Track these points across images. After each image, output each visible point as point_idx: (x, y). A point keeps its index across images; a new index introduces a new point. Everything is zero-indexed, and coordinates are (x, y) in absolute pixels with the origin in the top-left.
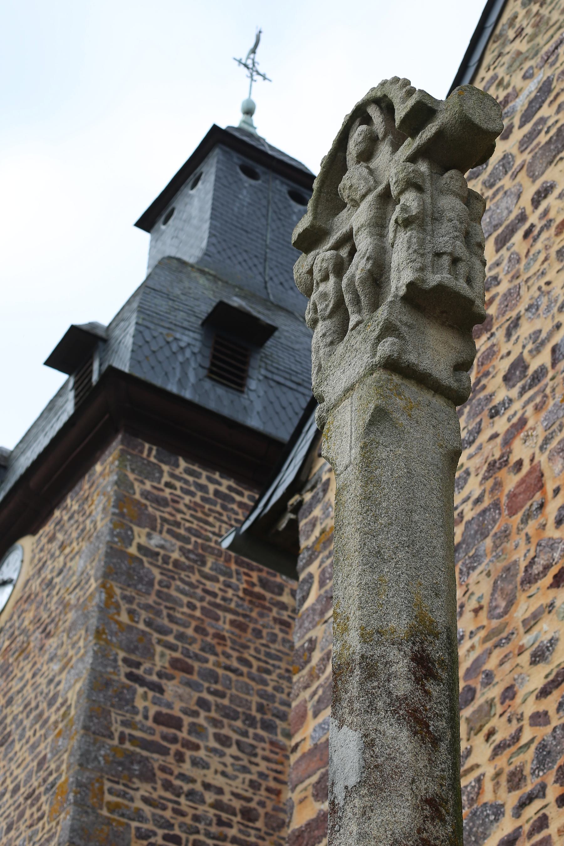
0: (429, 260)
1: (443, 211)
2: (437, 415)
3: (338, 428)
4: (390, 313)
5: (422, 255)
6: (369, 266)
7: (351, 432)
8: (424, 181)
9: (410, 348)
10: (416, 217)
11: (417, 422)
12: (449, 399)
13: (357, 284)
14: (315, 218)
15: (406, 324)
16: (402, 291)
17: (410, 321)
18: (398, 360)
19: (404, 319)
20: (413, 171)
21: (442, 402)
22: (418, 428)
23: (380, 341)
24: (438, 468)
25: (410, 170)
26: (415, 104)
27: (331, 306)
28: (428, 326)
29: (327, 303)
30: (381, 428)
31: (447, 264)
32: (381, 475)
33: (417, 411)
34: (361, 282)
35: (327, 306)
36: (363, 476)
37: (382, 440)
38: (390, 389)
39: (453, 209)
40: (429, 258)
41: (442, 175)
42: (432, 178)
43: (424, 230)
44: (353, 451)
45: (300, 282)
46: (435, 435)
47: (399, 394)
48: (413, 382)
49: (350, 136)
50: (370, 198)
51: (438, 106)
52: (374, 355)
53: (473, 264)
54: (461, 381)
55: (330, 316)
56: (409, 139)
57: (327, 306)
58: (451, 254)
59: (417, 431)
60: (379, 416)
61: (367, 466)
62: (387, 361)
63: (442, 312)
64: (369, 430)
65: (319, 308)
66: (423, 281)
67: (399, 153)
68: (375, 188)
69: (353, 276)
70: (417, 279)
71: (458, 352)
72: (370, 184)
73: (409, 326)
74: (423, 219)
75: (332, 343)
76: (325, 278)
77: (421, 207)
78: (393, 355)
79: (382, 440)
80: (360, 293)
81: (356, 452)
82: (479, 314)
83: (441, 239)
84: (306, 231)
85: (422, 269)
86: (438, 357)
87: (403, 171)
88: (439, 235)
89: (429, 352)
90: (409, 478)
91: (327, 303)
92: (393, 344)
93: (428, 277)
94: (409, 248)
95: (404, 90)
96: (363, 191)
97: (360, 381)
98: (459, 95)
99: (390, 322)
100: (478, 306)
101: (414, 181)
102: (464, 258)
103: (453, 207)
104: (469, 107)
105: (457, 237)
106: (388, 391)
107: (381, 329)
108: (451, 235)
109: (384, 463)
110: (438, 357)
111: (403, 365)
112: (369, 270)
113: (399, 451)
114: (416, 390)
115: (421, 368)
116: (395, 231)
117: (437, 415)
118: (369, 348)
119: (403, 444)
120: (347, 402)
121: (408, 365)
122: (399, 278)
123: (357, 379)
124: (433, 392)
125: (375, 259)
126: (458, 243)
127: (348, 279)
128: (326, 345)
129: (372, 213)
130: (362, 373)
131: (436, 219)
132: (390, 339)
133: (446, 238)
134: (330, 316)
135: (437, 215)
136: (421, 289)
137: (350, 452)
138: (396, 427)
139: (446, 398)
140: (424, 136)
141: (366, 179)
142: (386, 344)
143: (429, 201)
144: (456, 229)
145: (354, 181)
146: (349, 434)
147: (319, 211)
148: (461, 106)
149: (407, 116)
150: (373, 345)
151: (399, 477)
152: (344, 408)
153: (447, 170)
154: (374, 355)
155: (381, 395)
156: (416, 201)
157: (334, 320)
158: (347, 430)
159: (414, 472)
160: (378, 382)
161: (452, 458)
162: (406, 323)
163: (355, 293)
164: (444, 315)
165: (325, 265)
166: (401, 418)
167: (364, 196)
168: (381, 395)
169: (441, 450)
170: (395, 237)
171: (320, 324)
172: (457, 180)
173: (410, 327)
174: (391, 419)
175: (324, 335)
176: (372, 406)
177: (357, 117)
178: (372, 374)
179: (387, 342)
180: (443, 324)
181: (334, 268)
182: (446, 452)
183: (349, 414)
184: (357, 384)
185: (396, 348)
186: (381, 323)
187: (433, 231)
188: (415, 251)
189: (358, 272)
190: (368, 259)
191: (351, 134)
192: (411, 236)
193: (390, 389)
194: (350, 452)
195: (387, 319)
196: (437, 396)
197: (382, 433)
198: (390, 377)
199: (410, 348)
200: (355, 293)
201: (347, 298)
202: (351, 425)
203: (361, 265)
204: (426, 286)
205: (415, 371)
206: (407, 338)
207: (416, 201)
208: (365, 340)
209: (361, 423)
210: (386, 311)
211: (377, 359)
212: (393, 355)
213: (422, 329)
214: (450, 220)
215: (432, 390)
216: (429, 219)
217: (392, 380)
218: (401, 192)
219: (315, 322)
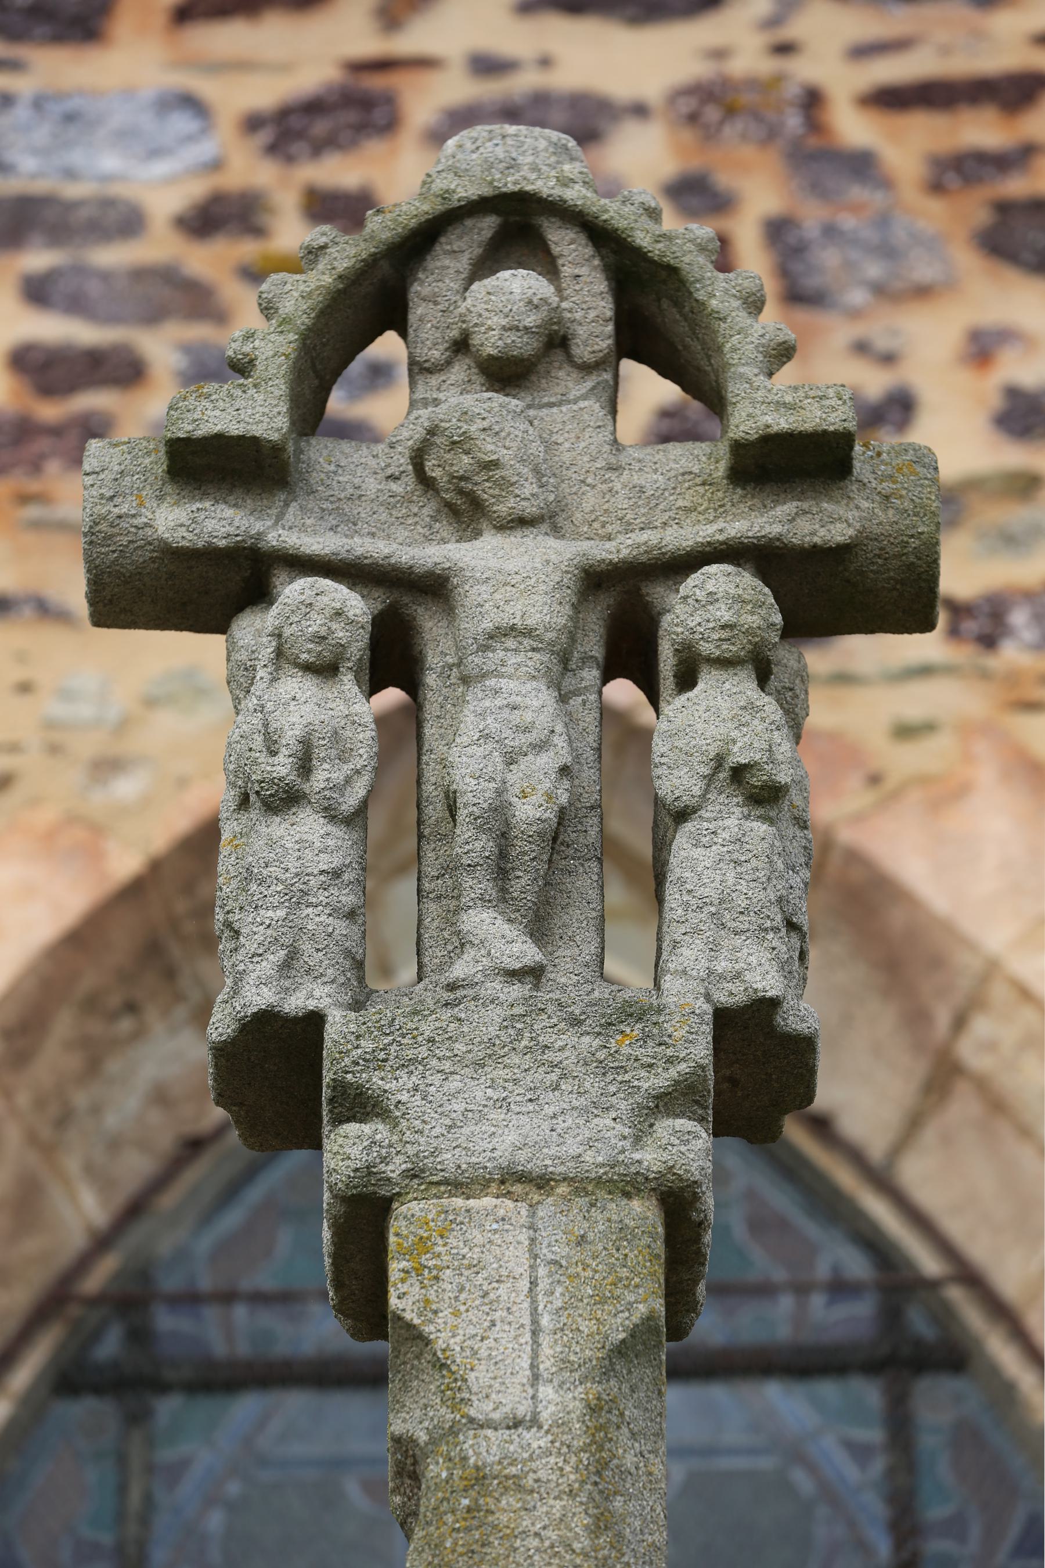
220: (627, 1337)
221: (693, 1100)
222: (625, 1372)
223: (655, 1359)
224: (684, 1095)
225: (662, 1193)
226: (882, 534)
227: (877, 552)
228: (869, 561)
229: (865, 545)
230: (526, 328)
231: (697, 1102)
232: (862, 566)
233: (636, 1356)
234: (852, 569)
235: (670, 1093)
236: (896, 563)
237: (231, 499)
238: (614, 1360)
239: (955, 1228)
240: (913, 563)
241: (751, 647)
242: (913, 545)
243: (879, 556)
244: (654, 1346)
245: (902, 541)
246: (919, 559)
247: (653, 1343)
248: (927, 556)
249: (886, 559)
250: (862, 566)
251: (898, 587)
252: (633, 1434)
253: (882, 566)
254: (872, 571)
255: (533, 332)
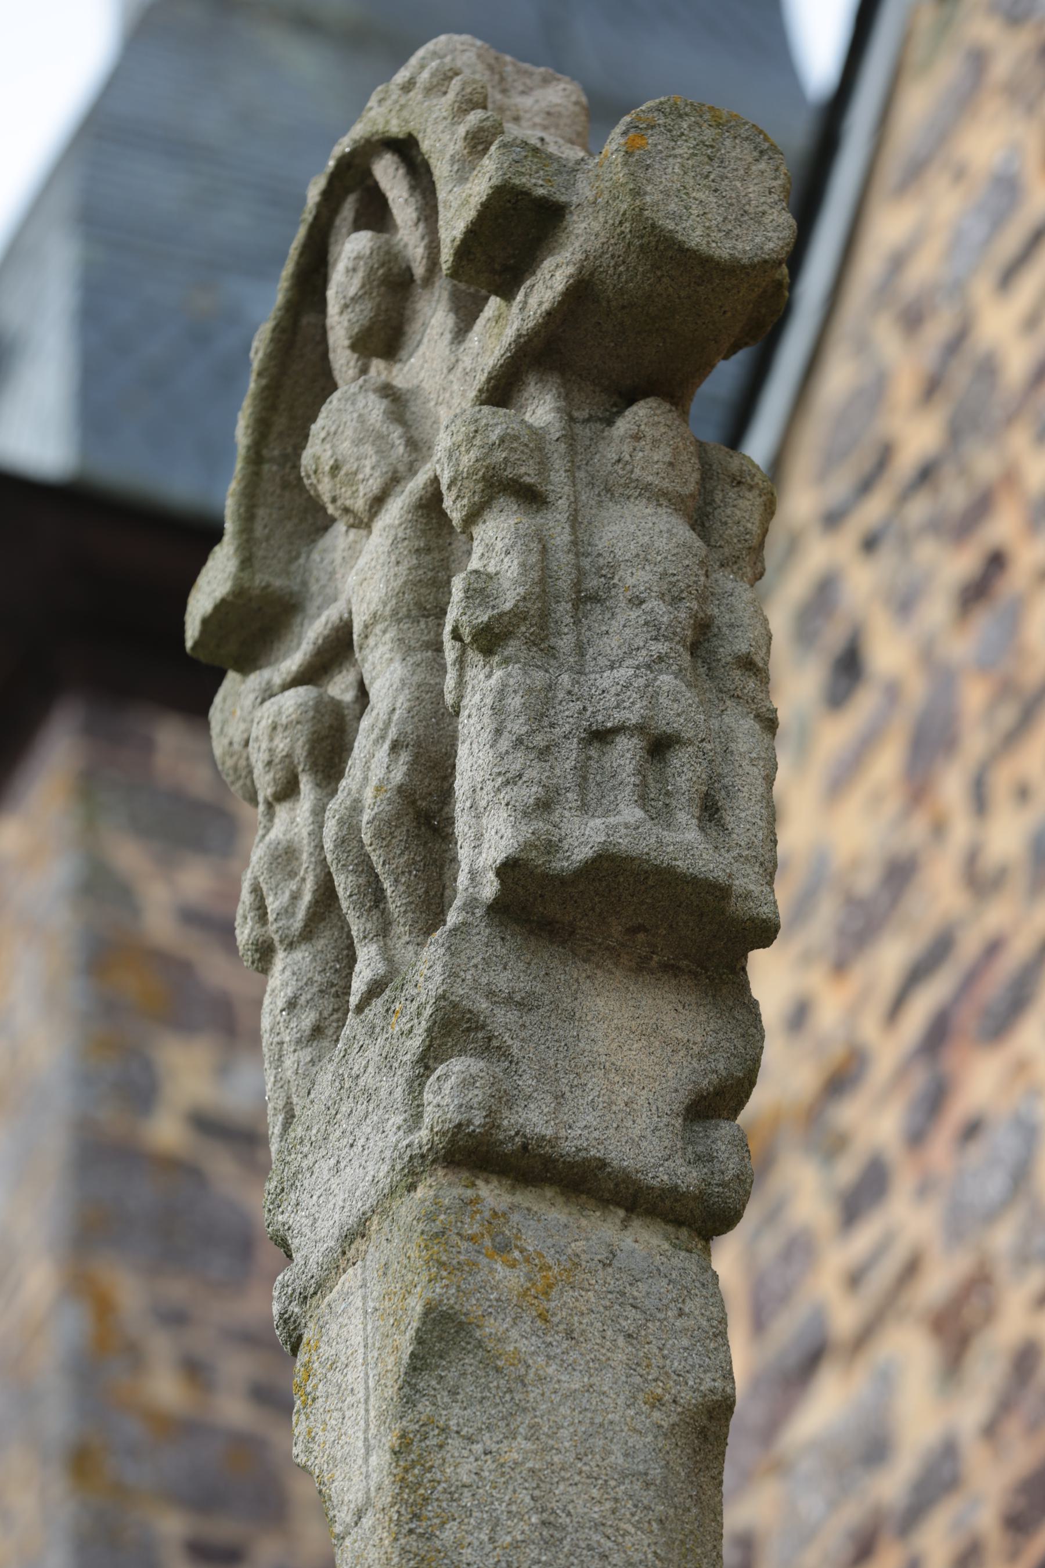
0: (569, 765)
1: (613, 567)
2: (638, 1292)
3: (333, 1367)
4: (452, 975)
5: (544, 753)
6: (398, 776)
7: (367, 1388)
8: (544, 466)
9: (527, 1082)
10: (518, 615)
11: (569, 1335)
12: (678, 1223)
13: (366, 839)
14: (246, 562)
15: (509, 1000)
16: (489, 889)
17: (523, 985)
18: (488, 1133)
19: (502, 981)
20: (502, 440)
21: (655, 1241)
22: (574, 1355)
23: (429, 1069)
24: (647, 1485)
25: (494, 437)
26: (490, 198)
27: (307, 897)
28: (586, 986)
29: (293, 885)
30: (452, 1376)
31: (630, 768)
32: (459, 1544)
33: (569, 1295)
34: (378, 835)
35: (295, 897)
36: (404, 1551)
37: (455, 1416)
38: (471, 1238)
39: (643, 557)
40: (570, 754)
41: (610, 422)
42: (572, 449)
43: (551, 652)
44: (374, 1460)
45: (235, 769)
46: (633, 1366)
47: (503, 1248)
48: (549, 1193)
49: (331, 259)
50: (395, 510)
51: (570, 185)
52: (416, 1119)
53: (727, 736)
54: (711, 1159)
55: (308, 934)
56: (494, 303)
57: (295, 897)
58: (641, 729)
59: (572, 1367)
60: (441, 1339)
61: (416, 1516)
62: (452, 1141)
63: (634, 930)
64: (413, 1386)
65: (273, 905)
66: (551, 847)
67: (474, 338)
68: (412, 470)
69: (356, 808)
70: (528, 846)
71: (700, 1056)
72: (393, 459)
73: (519, 1004)
74: (545, 614)
75: (317, 1032)
76: (288, 791)
77: (535, 575)
78: (469, 1122)
79: (455, 1416)
80: (379, 870)
81: (380, 1459)
82: (752, 920)
83: (607, 679)
84: (222, 607)
85: (544, 805)
86: (627, 1092)
87: (470, 440)
88: (603, 662)
89: (595, 1081)
90: (548, 1544)
91: (293, 885)
92: (468, 1082)
93: (566, 827)
94: (498, 732)
95: (462, 130)
96: (373, 485)
97: (381, 1207)
98: (628, 154)
99: (455, 1006)
100: (748, 896)
101: (509, 473)
102: (686, 735)
103: (646, 548)
104: (666, 193)
105: (660, 659)
106: (464, 1245)
107: (429, 1030)
108: (642, 657)
109: (467, 1500)
110: (627, 1092)
111: (509, 1148)
112: (400, 789)
113: (514, 1451)
114: (563, 1218)
115: (567, 1147)
116: (461, 662)
117: (638, 1292)
118: (398, 1093)
119: (523, 1423)
120: (350, 1278)
121: (525, 1147)
122: (479, 837)
123: (372, 1201)
124: (621, 1213)
125: (418, 744)
126: (666, 680)
127: (341, 822)
128: (299, 1041)
129: (403, 569)
130: (385, 1184)
131: (595, 598)
132: (457, 1066)
133: (623, 673)
134: (308, 934)
135: (593, 583)
136: (545, 876)
137: (366, 1460)
138: (498, 1370)
139: (667, 1221)
140: (533, 301)
141: (380, 439)
142: (447, 1086)
143: (561, 537)
144: (656, 630)
145: (345, 447)
146: (361, 1395)
147: (259, 532)
148: (637, 193)
149: (473, 233)
150: (410, 1082)
151: (516, 1545)
152: (346, 1295)
153: (629, 399)
154: (416, 1119)
155: (442, 1264)
156: (514, 554)
157: (320, 943)
158: (354, 1377)
159: (564, 1519)
160: (430, 1217)
161: (703, 1433)
162: (509, 999)
163: (365, 867)
164: (641, 937)
165: (281, 745)
166: (514, 1334)
167: (378, 502)
168: (442, 1264)
169: (656, 1415)
170: (461, 683)
171: (280, 959)
172: (655, 443)
173: (524, 1005)
174: (480, 1345)
175: (292, 1005)
176: (416, 1306)
177: (348, 191)
178: (412, 1187)
179: (447, 1076)
180: (641, 968)
181: (310, 753)
182: (674, 1418)
183: (357, 1320)
184: (376, 1219)
185: (477, 1095)
186: (428, 1011)
187: (580, 649)
188: (519, 742)
189: (369, 793)
190: (395, 747)
191: (333, 250)
192: (505, 685)
193: (471, 1238)
194: (366, 1460)
195: (443, 997)
196: (636, 1223)
197: (453, 1393)
198: (469, 1193)
199: (527, 1082)
200: (365, 867)
201: (343, 884)
202: (365, 1363)
203: (377, 773)
204: (561, 864)
205: (548, 1162)
206: (515, 1051)
207: (514, 554)
208: (388, 1060)
209: (391, 1360)
210: (439, 968)
211: (423, 1134)
212: (469, 1122)
213: (567, 1003)
214: (637, 601)
215: (618, 1204)
216: (563, 609)
217: (476, 1200)
218: (473, 517)
219: (264, 952)
220: (415, 1349)
221: (463, 1031)
222: (433, 1383)
223: (468, 1343)
224: (449, 1034)
225: (445, 1157)
226: (603, 244)
227: (612, 263)
228: (615, 277)
229: (600, 266)
230: (352, 299)
231: (468, 1029)
232: (615, 286)
233: (441, 1357)
234: (611, 295)
235: (430, 1046)
236: (632, 258)
237: (273, 658)
238: (414, 1381)
240: (641, 246)
241: (480, 485)
242: (628, 230)
243: (616, 266)
244: (456, 1332)
245: (619, 235)
246: (642, 237)
247: (452, 1331)
248: (645, 228)
249: (624, 262)
250: (615, 286)
251: (659, 273)
252: (469, 1439)
253: (627, 269)
254: (627, 282)
255: (360, 297)
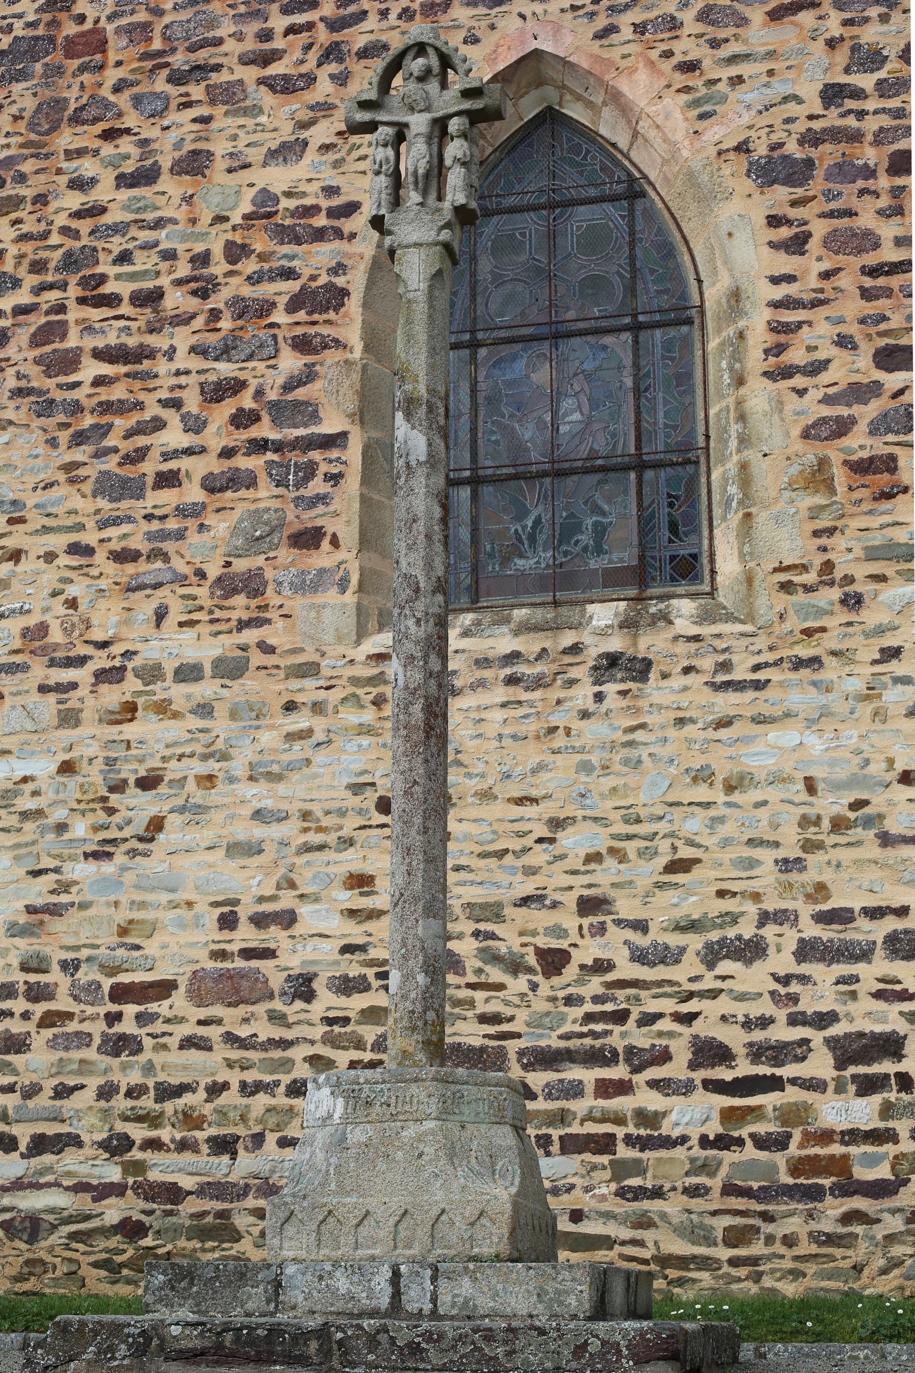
239: (641, 166)
